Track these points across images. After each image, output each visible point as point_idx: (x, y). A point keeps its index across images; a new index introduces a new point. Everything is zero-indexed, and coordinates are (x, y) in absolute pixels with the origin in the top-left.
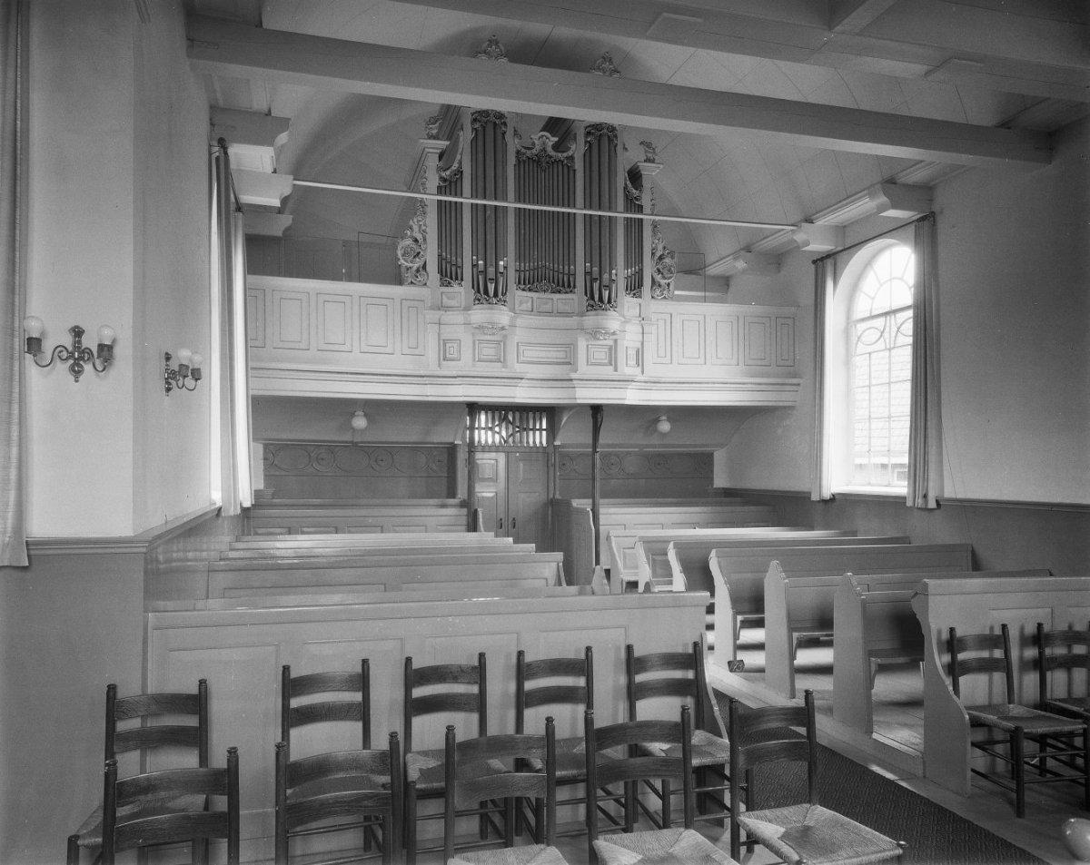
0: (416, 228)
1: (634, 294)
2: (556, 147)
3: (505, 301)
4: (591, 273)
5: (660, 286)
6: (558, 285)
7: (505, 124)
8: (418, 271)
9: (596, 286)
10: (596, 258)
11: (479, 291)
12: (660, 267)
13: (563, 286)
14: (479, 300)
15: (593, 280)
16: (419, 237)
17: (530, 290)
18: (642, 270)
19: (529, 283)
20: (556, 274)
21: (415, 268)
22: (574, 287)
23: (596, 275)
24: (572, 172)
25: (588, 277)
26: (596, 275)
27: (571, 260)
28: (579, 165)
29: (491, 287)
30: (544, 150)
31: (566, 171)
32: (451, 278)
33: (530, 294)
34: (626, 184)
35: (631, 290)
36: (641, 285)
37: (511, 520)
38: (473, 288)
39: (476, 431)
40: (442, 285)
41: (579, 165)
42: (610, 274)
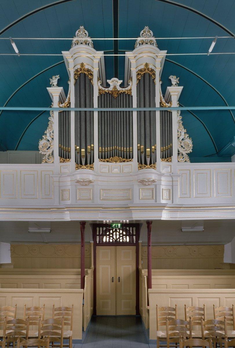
0: (48, 135)
1: (167, 160)
2: (122, 86)
3: (155, 167)
4: (61, 147)
5: (182, 155)
6: (124, 158)
7: (91, 75)
8: (49, 156)
9: (143, 155)
10: (143, 143)
11: (141, 163)
12: (182, 144)
13: (127, 158)
14: (141, 167)
15: (141, 153)
16: (50, 139)
17: (108, 161)
18: (172, 147)
19: (108, 158)
20: (118, 151)
21: (47, 155)
22: (133, 158)
23: (62, 148)
24: (130, 98)
25: (139, 151)
26: (142, 150)
27: (131, 144)
28: (134, 94)
29: (148, 160)
30: (115, 87)
31: (111, 96)
32: (127, 158)
33: (108, 163)
34: (161, 100)
35: (165, 158)
36: (171, 155)
37: (118, 278)
38: (138, 162)
39: (98, 237)
40: (61, 162)
41: (134, 94)
42: (151, 148)
